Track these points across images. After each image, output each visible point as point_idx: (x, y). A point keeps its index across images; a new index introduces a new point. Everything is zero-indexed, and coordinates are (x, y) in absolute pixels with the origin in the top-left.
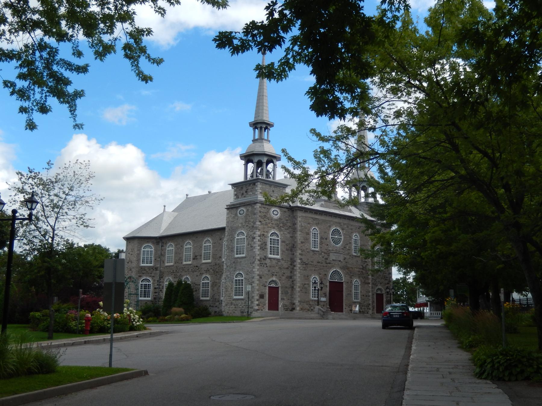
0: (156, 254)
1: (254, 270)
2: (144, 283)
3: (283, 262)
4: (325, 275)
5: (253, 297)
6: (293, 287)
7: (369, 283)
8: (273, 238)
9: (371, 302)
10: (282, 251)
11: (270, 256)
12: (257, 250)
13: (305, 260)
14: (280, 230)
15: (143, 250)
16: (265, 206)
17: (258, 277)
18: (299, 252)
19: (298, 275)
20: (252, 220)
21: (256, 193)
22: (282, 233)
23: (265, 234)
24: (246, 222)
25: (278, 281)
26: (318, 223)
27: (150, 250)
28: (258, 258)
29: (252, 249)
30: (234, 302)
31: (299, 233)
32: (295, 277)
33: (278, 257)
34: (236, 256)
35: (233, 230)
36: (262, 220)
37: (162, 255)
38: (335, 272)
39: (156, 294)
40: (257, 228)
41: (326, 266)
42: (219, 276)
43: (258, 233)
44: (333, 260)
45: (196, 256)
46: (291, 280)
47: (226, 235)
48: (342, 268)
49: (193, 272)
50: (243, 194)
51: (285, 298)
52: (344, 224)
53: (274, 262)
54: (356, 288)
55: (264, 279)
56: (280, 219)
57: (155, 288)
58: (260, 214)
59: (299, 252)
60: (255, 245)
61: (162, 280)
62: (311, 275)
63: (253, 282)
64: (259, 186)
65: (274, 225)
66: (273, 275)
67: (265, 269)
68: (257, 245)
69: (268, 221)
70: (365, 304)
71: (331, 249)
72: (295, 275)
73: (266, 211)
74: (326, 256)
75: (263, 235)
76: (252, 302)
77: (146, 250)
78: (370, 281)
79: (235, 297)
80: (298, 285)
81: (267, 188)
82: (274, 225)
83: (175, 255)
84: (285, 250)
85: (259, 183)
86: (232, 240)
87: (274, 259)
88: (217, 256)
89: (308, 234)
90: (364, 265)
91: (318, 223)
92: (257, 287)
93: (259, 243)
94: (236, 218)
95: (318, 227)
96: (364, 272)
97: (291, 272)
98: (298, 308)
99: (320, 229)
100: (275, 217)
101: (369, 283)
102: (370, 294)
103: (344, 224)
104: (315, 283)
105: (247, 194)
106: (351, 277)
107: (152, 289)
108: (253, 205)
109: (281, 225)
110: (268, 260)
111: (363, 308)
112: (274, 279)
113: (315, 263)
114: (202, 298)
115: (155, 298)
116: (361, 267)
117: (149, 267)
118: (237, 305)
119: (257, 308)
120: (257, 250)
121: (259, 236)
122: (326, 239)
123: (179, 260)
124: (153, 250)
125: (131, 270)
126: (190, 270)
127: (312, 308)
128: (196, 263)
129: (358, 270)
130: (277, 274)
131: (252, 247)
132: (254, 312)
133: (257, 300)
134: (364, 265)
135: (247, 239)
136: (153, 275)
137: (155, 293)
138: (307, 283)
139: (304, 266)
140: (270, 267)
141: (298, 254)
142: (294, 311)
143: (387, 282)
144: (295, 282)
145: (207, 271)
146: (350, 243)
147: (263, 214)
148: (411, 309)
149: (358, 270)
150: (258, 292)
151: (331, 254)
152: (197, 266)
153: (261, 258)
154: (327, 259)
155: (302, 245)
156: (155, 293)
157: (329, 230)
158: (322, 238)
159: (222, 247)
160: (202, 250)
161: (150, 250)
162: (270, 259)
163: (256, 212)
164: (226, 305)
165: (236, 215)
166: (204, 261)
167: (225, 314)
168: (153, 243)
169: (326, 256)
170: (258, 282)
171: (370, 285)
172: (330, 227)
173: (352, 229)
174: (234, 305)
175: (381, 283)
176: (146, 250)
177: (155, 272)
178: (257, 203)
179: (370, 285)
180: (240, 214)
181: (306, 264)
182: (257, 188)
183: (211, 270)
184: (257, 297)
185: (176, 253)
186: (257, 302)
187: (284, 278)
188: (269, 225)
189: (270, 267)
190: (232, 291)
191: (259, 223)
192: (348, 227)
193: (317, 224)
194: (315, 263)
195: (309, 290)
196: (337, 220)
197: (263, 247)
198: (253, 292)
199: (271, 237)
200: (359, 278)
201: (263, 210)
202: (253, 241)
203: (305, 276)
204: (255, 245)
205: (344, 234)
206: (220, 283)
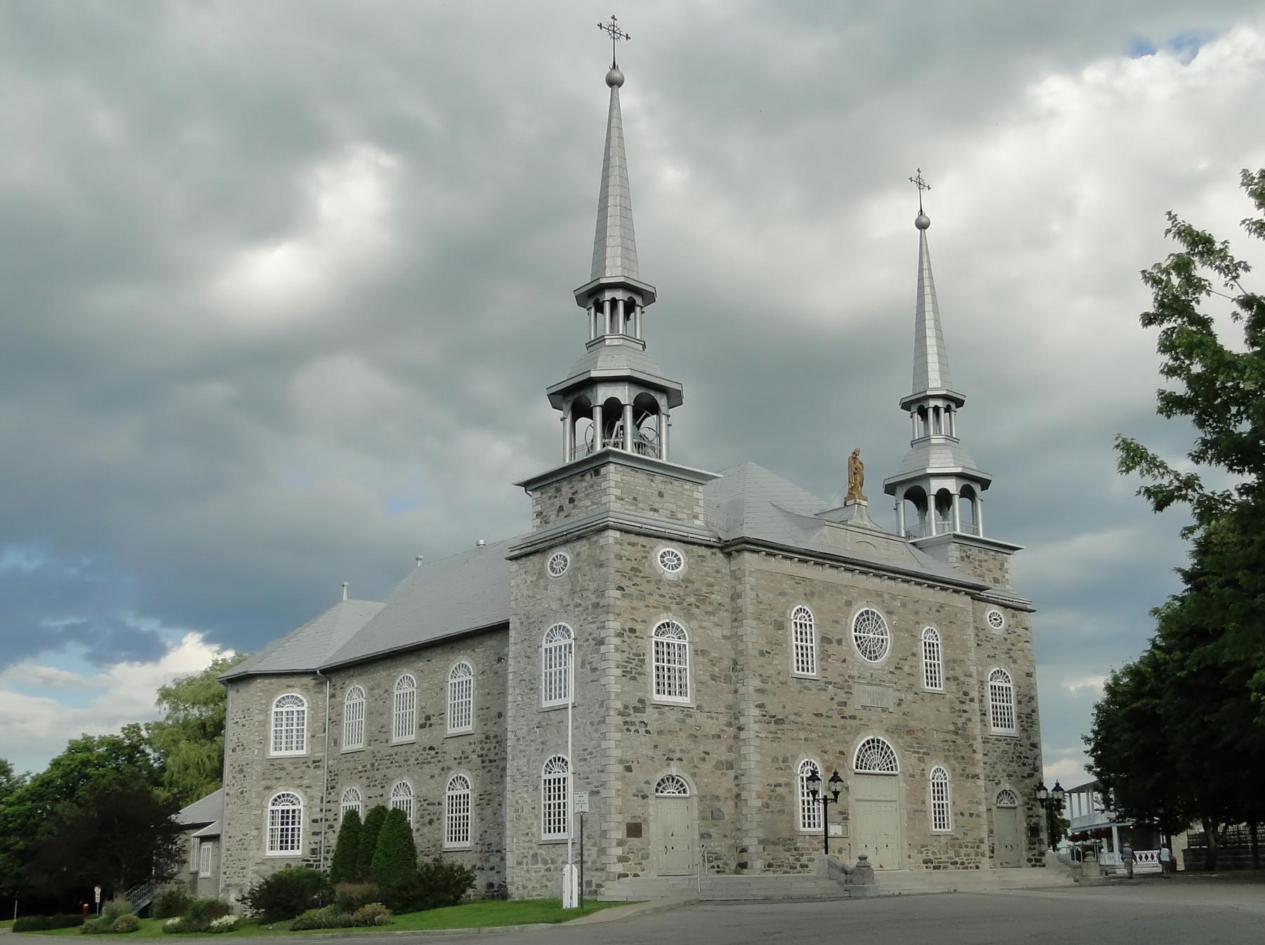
0: (313, 719)
1: (604, 744)
2: (280, 808)
3: (700, 717)
4: (842, 753)
5: (604, 834)
6: (738, 796)
7: (976, 776)
8: (664, 639)
9: (985, 835)
10: (699, 683)
11: (658, 698)
12: (613, 679)
13: (774, 708)
14: (689, 617)
15: (274, 709)
16: (633, 538)
17: (620, 768)
18: (755, 682)
19: (754, 757)
20: (592, 586)
21: (604, 500)
22: (694, 624)
23: (638, 627)
24: (573, 592)
25: (686, 776)
26: (812, 594)
27: (295, 709)
28: (618, 705)
29: (594, 676)
30: (542, 852)
31: (750, 623)
32: (744, 765)
33: (686, 700)
34: (546, 704)
35: (534, 624)
36: (625, 583)
37: (335, 722)
38: (872, 744)
39: (317, 838)
40: (607, 609)
41: (844, 727)
42: (498, 773)
43: (614, 625)
44: (864, 707)
45: (428, 718)
46: (731, 773)
47: (512, 640)
48: (893, 731)
49: (421, 764)
50: (561, 508)
51: (713, 831)
52: (894, 598)
53: (672, 717)
54: (939, 789)
55: (638, 776)
56: (687, 580)
57: (315, 821)
58: (618, 564)
59: (755, 682)
60: (604, 665)
61: (333, 796)
62: (794, 757)
63: (603, 785)
64: (612, 473)
65: (667, 601)
66: (669, 759)
67: (643, 739)
68: (612, 664)
69: (645, 587)
70: (969, 839)
71: (855, 673)
72: (743, 757)
73: (639, 556)
74: (841, 696)
75: (632, 630)
76: (602, 851)
77: (284, 709)
78: (979, 770)
79: (546, 837)
80: (756, 787)
81: (639, 480)
82: (667, 601)
83: (367, 718)
84: (706, 678)
85: (611, 467)
86: (530, 655)
87: (672, 707)
88: (493, 714)
89: (780, 626)
90: (960, 722)
91: (812, 594)
92: (618, 802)
93: (618, 657)
94: (542, 583)
95: (811, 606)
96: (960, 741)
97: (730, 749)
98: (758, 864)
99: (817, 610)
100: (670, 574)
101: (976, 776)
102: (983, 808)
103: (894, 598)
104: (814, 777)
105: (574, 507)
106: (921, 760)
107: (303, 825)
108: (595, 538)
109: (692, 599)
110: (649, 710)
111: (963, 851)
112: (674, 770)
113: (807, 718)
114: (448, 845)
115: (314, 851)
116: (952, 728)
117: (295, 761)
118: (553, 862)
119: (618, 868)
120: (613, 679)
121: (620, 635)
122: (839, 642)
123: (379, 733)
124: (305, 708)
125: (241, 771)
126: (412, 761)
127: (804, 860)
128: (428, 737)
129: (942, 736)
130: (684, 756)
131: (594, 670)
132: (608, 884)
133: (620, 843)
134: (960, 722)
135: (579, 647)
136: (306, 782)
137: (315, 834)
138: (783, 780)
139: (773, 727)
140: (660, 732)
141: (751, 690)
142: (746, 875)
143: (1027, 770)
144: (744, 780)
145: (462, 760)
146: (914, 655)
147: (629, 565)
148: (98, 890)
149: (942, 736)
150: (619, 818)
151: (856, 689)
152: (431, 748)
153: (626, 707)
154: (845, 704)
155: (762, 660)
156: (315, 834)
157: (847, 615)
158: (825, 640)
159: (505, 683)
160: (444, 698)
161: (295, 709)
162: (658, 707)
163: (603, 557)
164: (519, 863)
165: (541, 574)
166: (451, 731)
167: (515, 892)
168: (305, 689)
169: (841, 696)
170: (618, 785)
171: (981, 782)
172: (849, 604)
173: (917, 613)
174: (545, 862)
175: (1009, 776)
176: (284, 709)
177: (311, 772)
178: (607, 528)
179: (981, 782)
180: (553, 569)
181: (779, 722)
182: (604, 485)
183: (473, 757)
184: (620, 834)
185: (370, 713)
186: (619, 851)
187: (707, 767)
188: (651, 600)
189: (660, 732)
190: (537, 817)
191: (618, 594)
192: (904, 605)
193: (809, 596)
194: (807, 718)
195: (793, 803)
196: (872, 582)
197: (633, 670)
198: (603, 817)
199: (660, 639)
200: (947, 759)
201: (627, 551)
202: (598, 651)
203: (775, 759)
204: (604, 665)
205: (895, 629)
206: (501, 794)
